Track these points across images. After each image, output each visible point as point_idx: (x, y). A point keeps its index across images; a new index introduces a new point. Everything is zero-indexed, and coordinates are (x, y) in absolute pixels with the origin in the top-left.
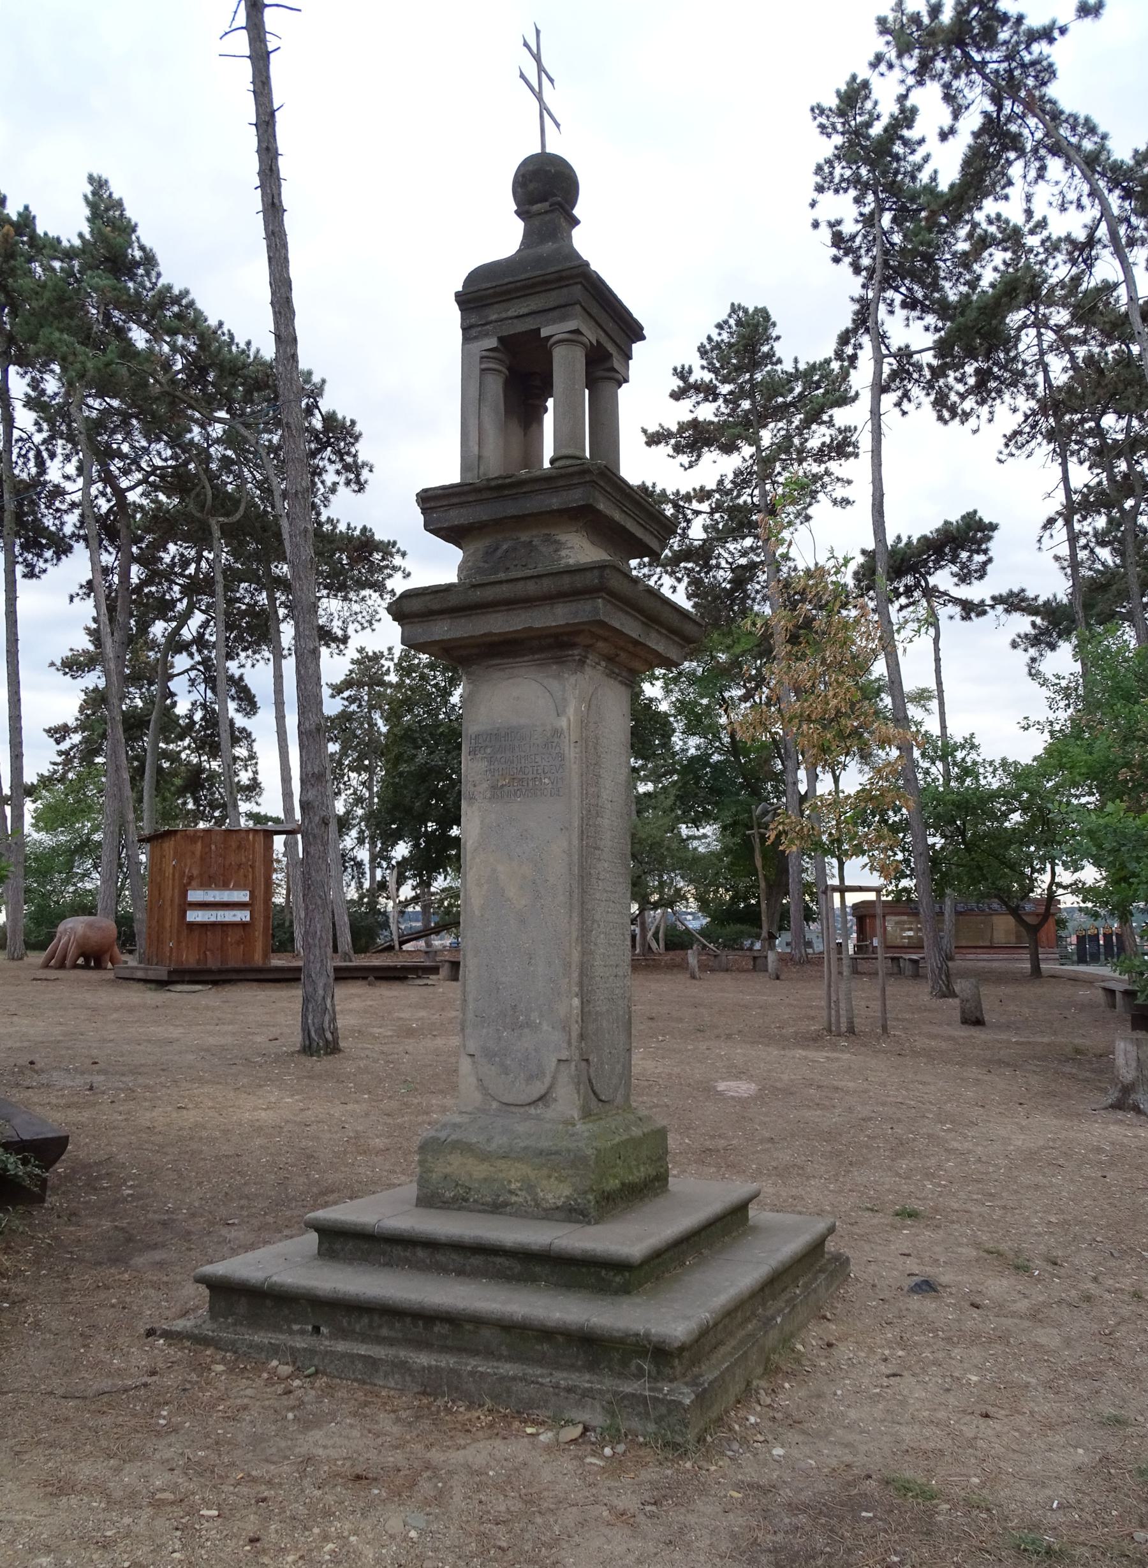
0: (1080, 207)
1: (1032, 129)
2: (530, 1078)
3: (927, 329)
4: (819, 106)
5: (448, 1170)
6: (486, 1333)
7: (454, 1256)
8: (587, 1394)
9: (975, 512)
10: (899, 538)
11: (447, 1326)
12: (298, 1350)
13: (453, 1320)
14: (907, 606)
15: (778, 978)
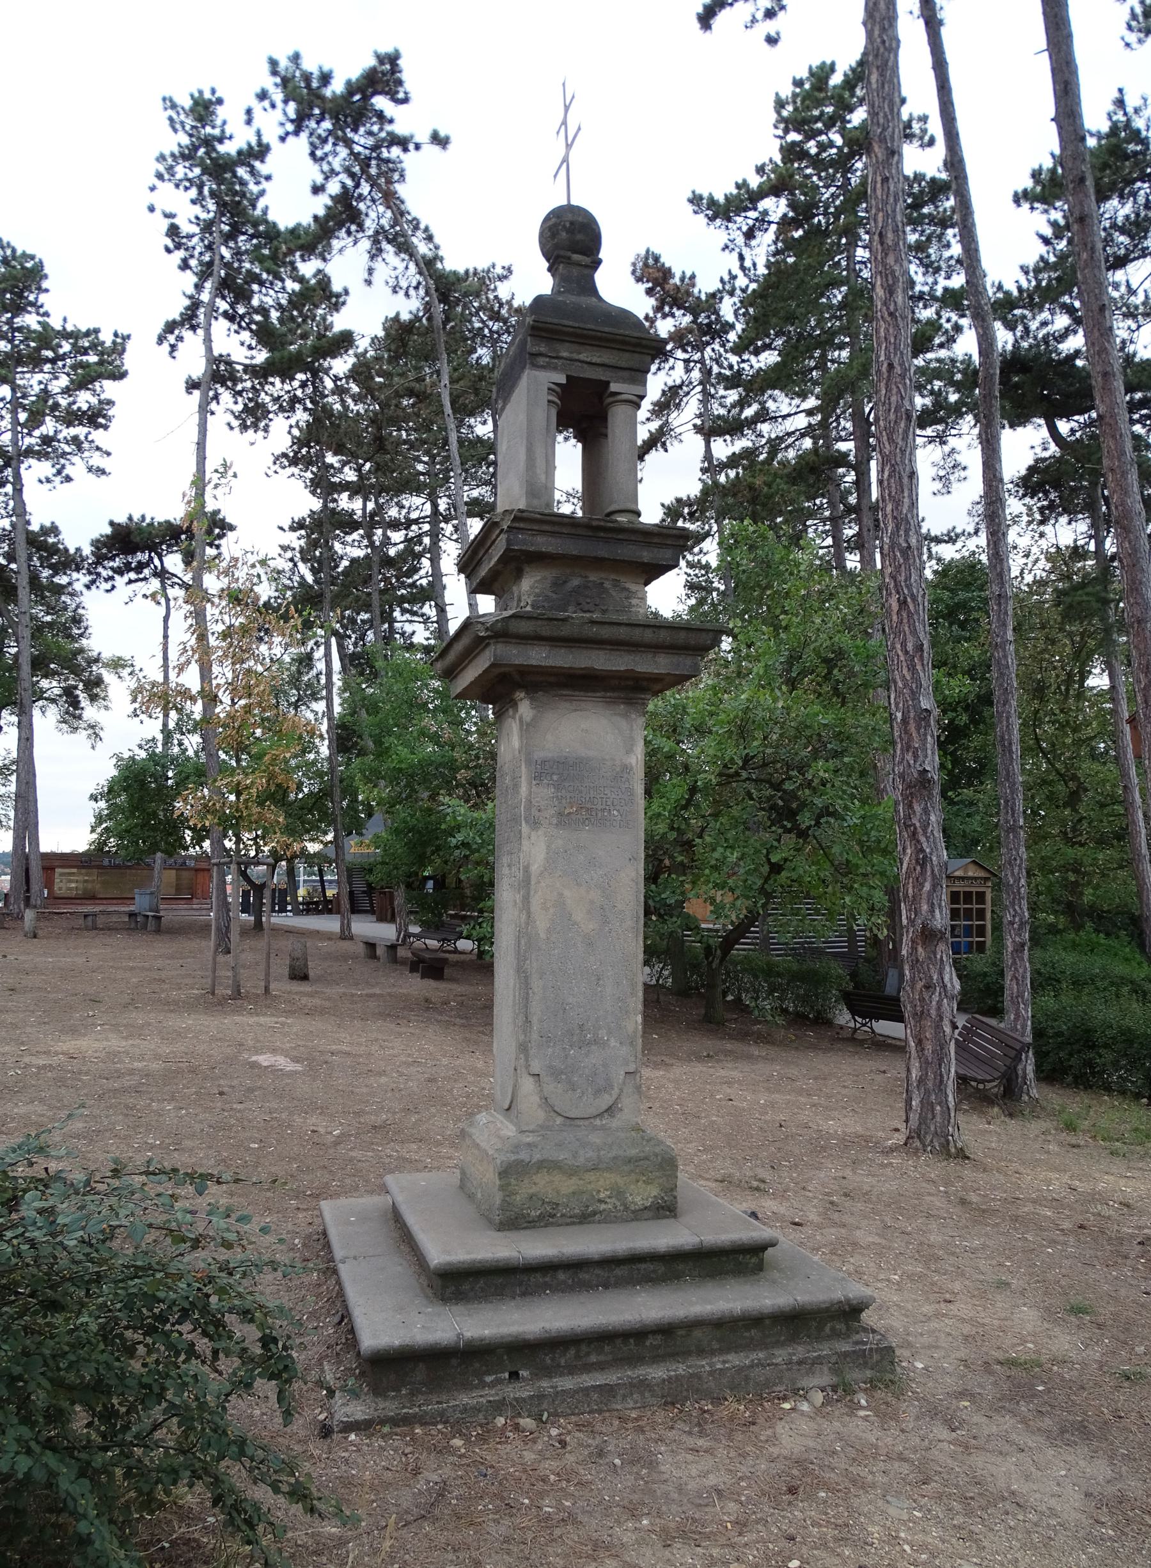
0: (407, 295)
1: (376, 216)
2: (598, 1092)
3: (242, 344)
4: (171, 100)
5: (534, 1190)
6: (697, 1333)
7: (597, 1271)
8: (818, 1360)
9: (219, 511)
10: (143, 517)
11: (659, 1337)
12: (524, 1400)
13: (667, 1330)
14: (136, 581)
15: (35, 936)
